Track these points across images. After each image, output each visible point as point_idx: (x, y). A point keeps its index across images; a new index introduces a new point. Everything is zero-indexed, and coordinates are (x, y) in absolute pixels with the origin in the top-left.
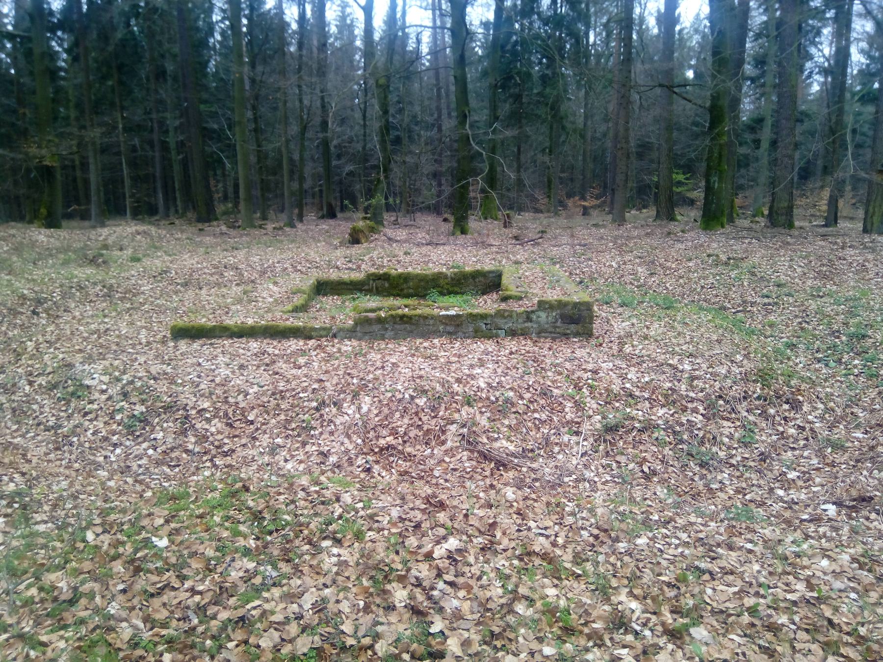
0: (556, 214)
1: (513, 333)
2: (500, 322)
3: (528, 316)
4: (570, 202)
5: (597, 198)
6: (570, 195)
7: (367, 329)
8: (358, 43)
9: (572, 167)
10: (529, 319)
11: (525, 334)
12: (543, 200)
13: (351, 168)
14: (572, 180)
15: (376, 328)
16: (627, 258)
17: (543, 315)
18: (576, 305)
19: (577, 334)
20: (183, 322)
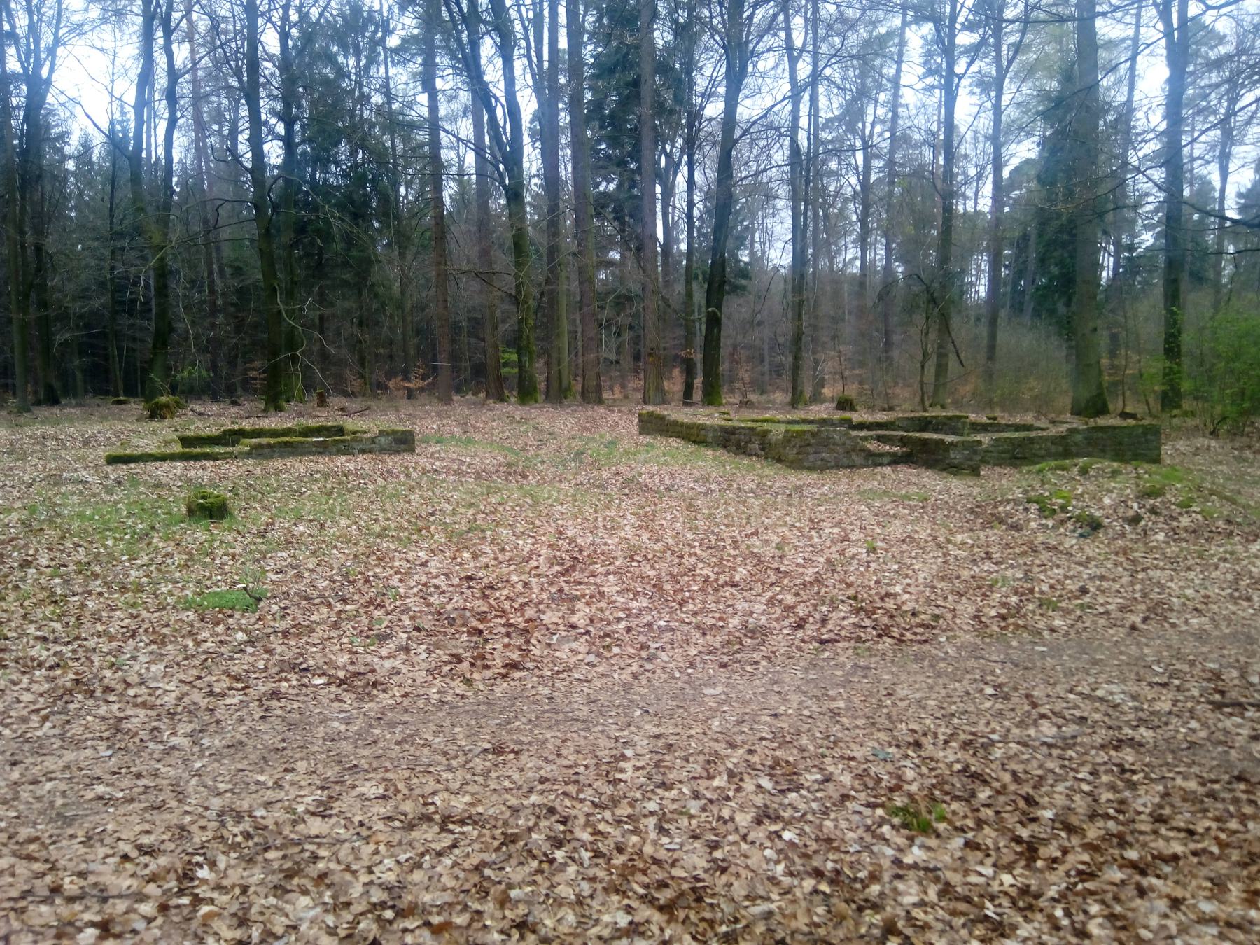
0: (375, 396)
1: (363, 452)
2: (355, 445)
3: (373, 440)
4: (391, 384)
5: (423, 379)
6: (391, 374)
7: (260, 451)
8: (15, 123)
9: (391, 343)
10: (373, 442)
11: (371, 451)
12: (356, 384)
13: (68, 336)
14: (391, 357)
15: (267, 451)
16: (445, 422)
17: (383, 439)
18: (403, 432)
19: (405, 451)
20: (117, 451)
